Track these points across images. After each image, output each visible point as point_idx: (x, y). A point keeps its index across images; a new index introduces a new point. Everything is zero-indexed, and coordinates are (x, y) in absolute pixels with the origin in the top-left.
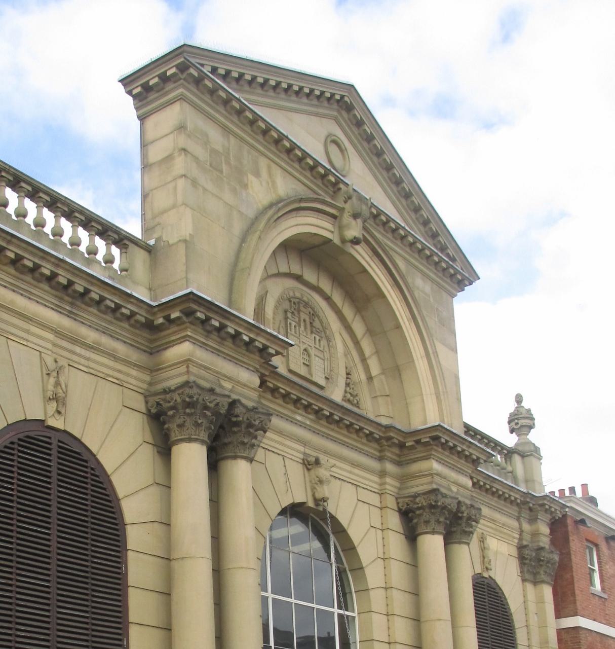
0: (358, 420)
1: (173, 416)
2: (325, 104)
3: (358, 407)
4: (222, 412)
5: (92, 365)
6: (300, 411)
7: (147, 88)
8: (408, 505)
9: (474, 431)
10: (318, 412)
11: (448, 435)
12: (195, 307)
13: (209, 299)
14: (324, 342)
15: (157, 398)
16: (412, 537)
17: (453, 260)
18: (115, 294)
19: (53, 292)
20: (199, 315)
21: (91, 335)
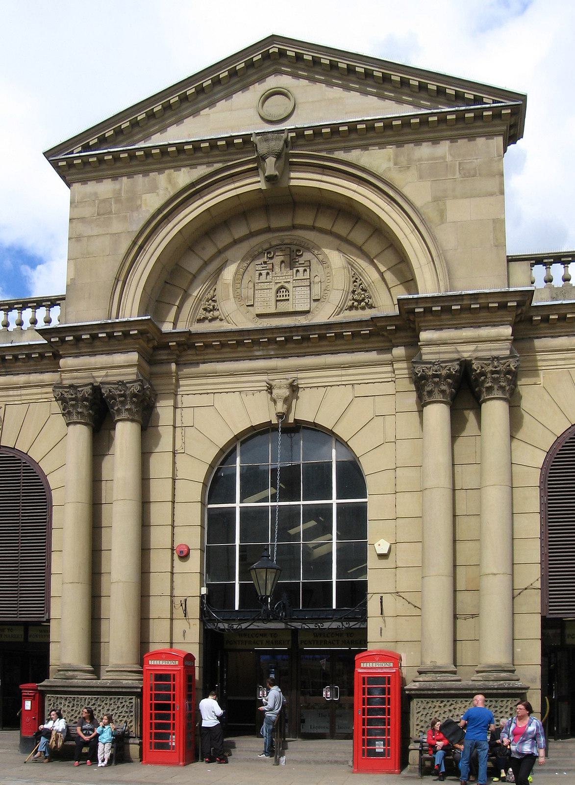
5: (24, 397)
8: (482, 368)
16: (422, 404)
18: (22, 349)
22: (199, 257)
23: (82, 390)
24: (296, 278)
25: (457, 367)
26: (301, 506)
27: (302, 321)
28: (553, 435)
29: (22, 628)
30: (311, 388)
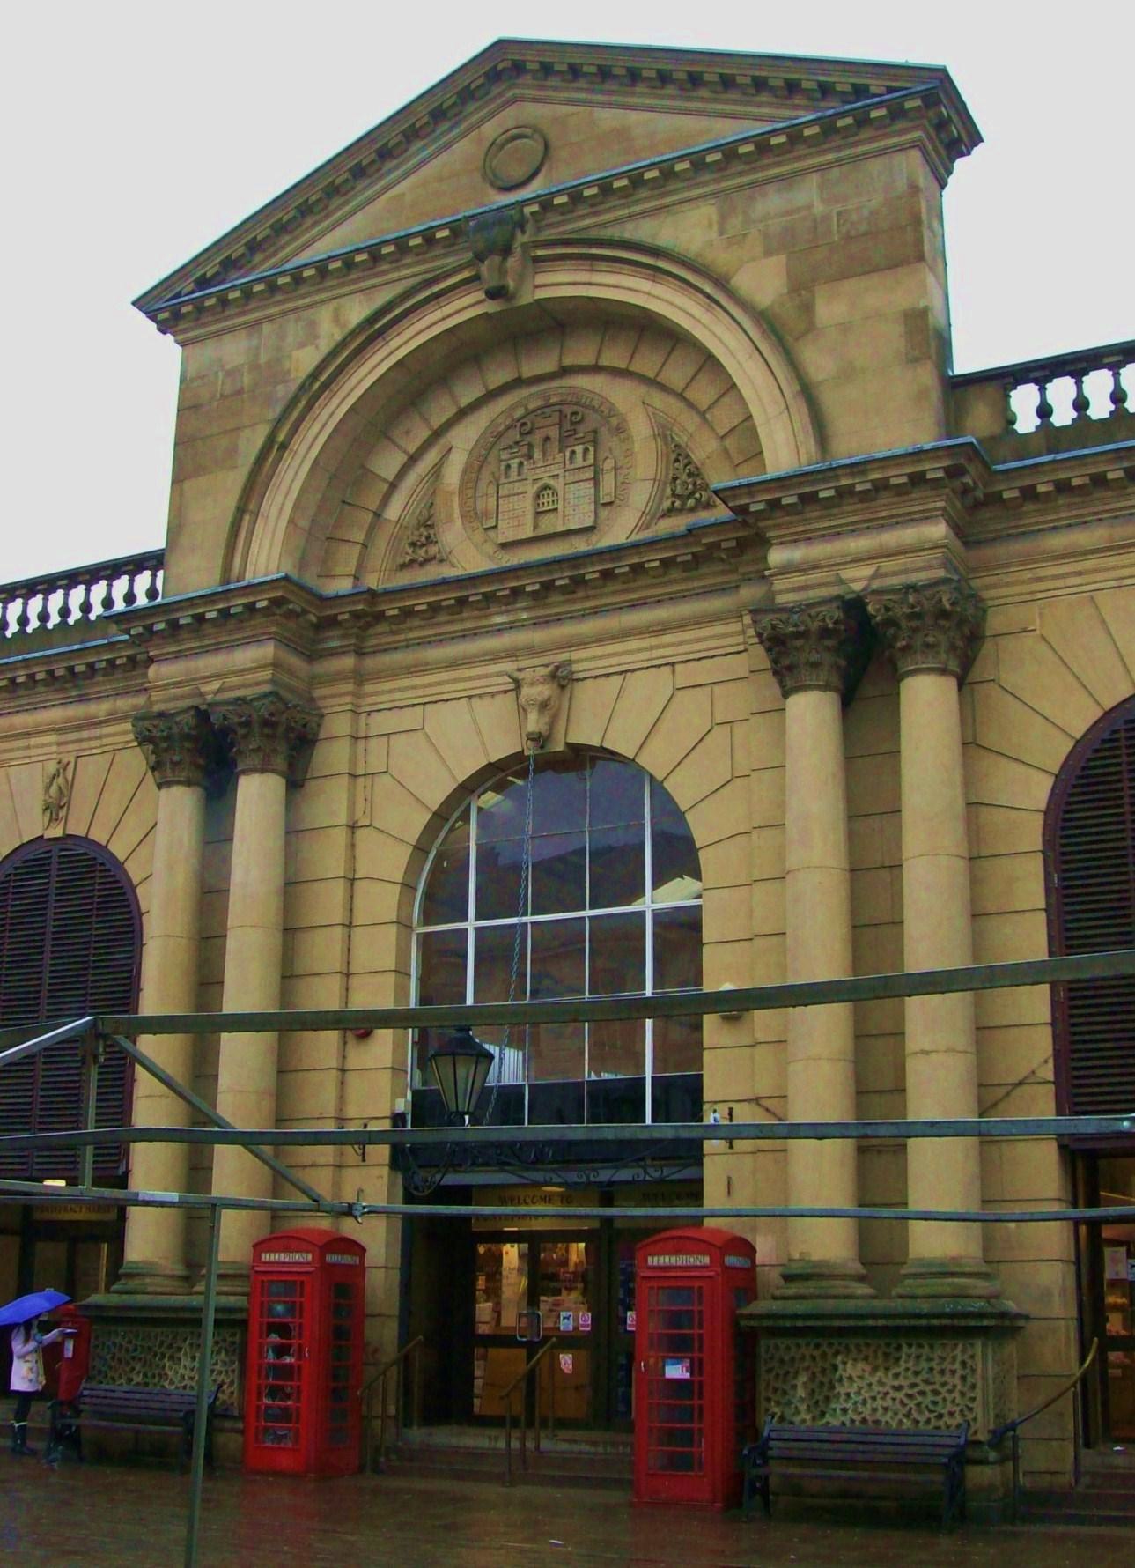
8: (887, 609)
19: (52, 688)
22: (400, 447)
23: (818, 614)
24: (572, 467)
25: (838, 614)
26: (529, 926)
27: (580, 545)
28: (1069, 739)
30: (596, 677)
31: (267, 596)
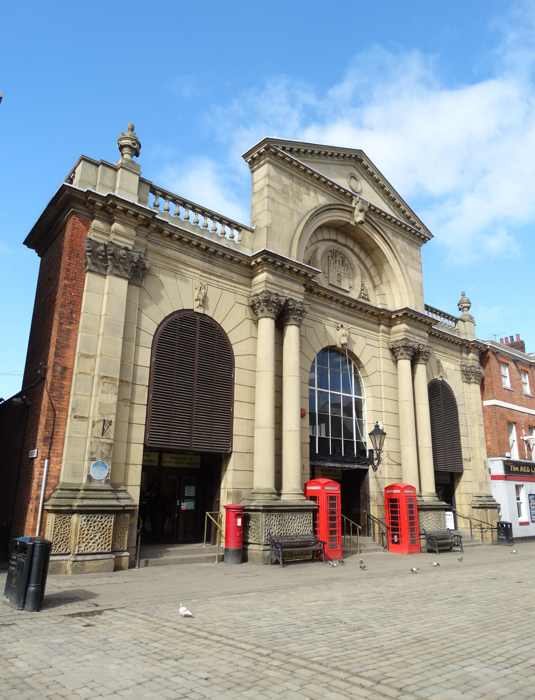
0: (365, 306)
1: (259, 306)
2: (348, 159)
3: (369, 300)
4: (282, 304)
6: (333, 303)
7: (254, 159)
9: (435, 310)
10: (343, 303)
11: (412, 312)
12: (268, 257)
13: (274, 252)
14: (350, 270)
15: (252, 298)
17: (419, 229)
19: (201, 252)
20: (269, 260)
21: (219, 271)
29: (157, 454)
31: (147, 215)
